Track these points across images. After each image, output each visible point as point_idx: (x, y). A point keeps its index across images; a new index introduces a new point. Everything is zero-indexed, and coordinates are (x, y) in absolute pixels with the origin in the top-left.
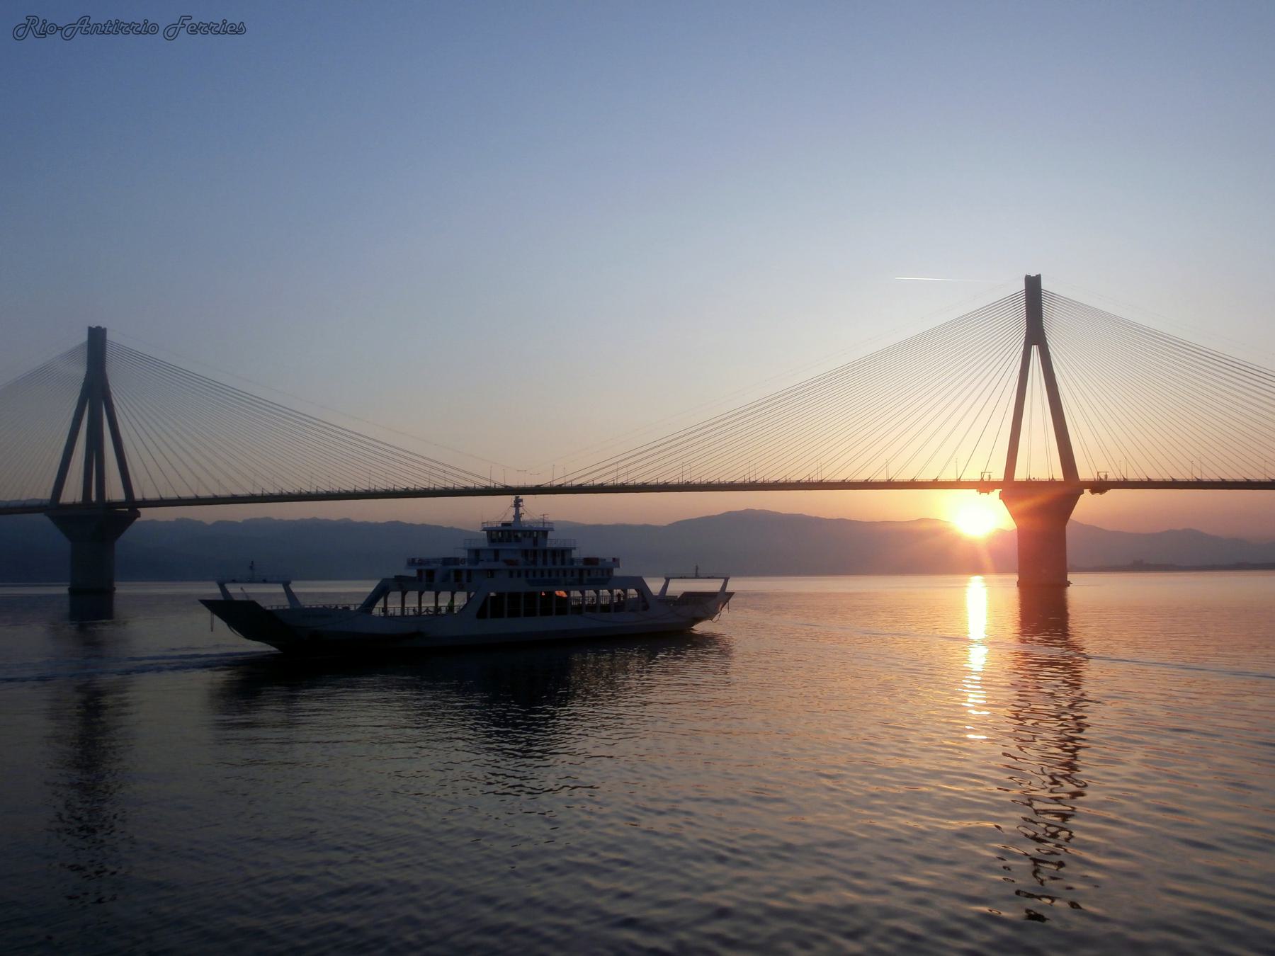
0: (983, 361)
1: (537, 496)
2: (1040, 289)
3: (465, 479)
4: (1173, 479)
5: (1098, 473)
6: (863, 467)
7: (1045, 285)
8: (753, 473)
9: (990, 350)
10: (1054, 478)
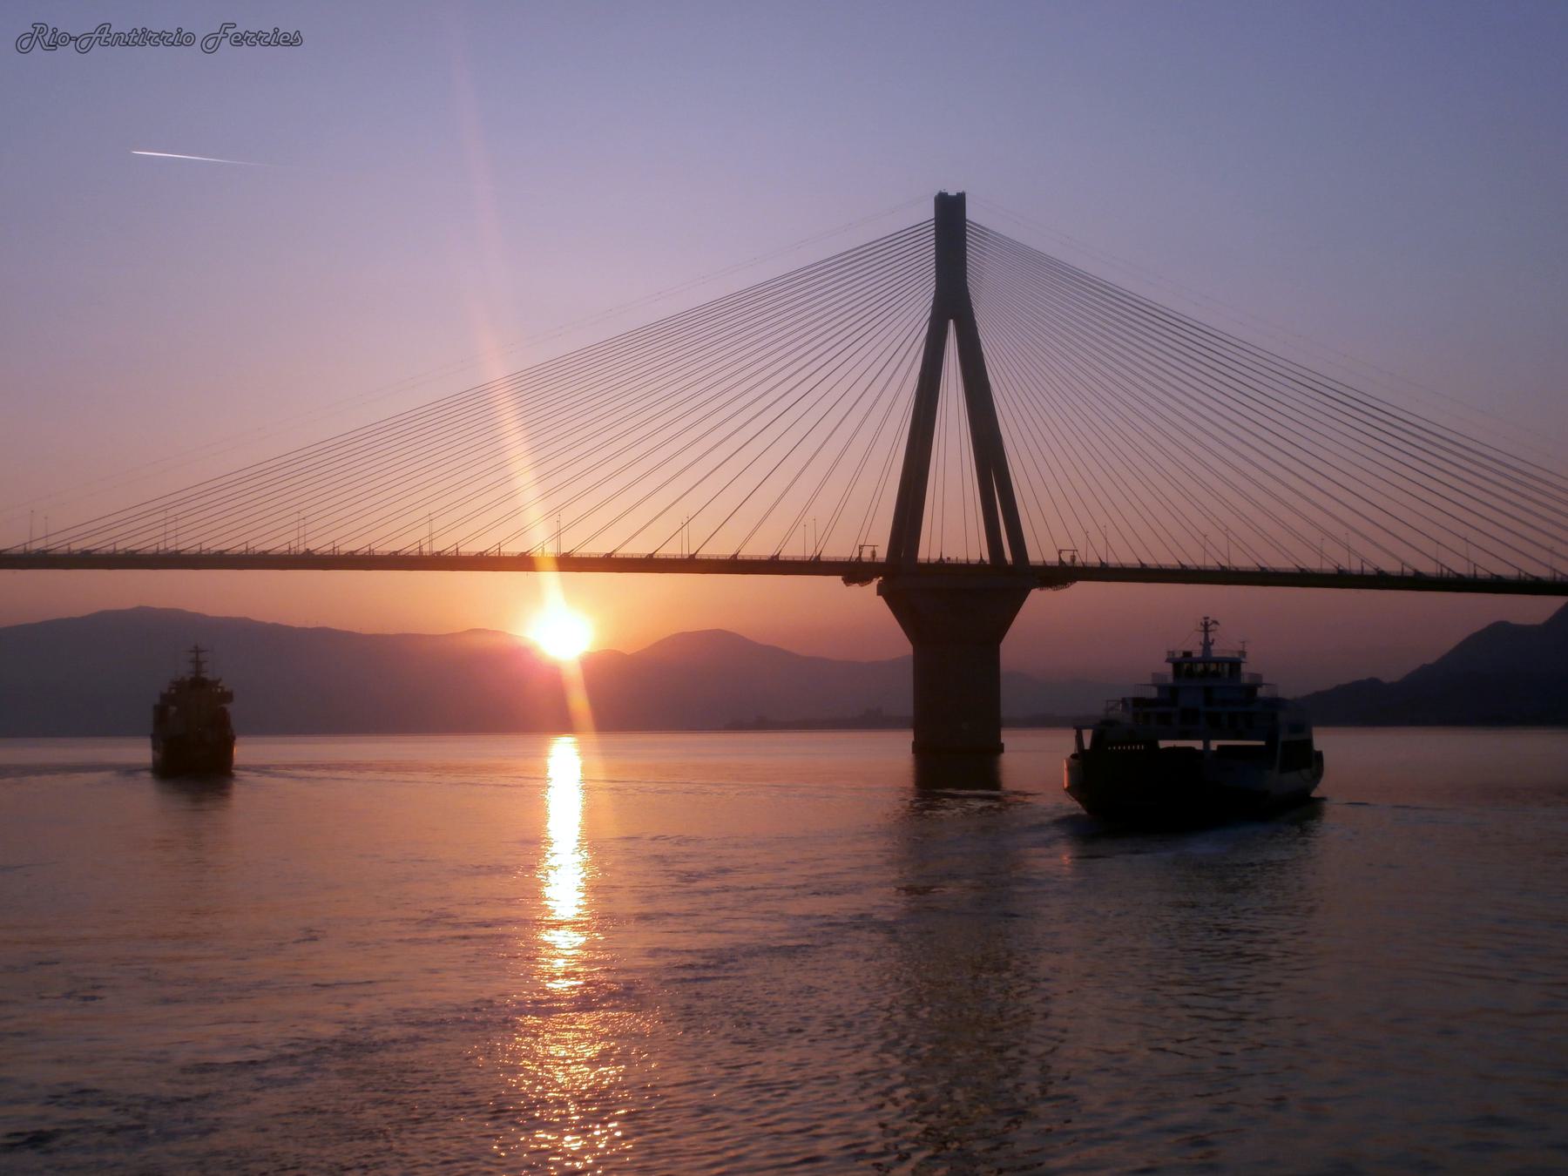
4: (1142, 564)
5: (1060, 552)
6: (113, 526)
7: (973, 213)
8: (302, 541)
9: (686, 342)
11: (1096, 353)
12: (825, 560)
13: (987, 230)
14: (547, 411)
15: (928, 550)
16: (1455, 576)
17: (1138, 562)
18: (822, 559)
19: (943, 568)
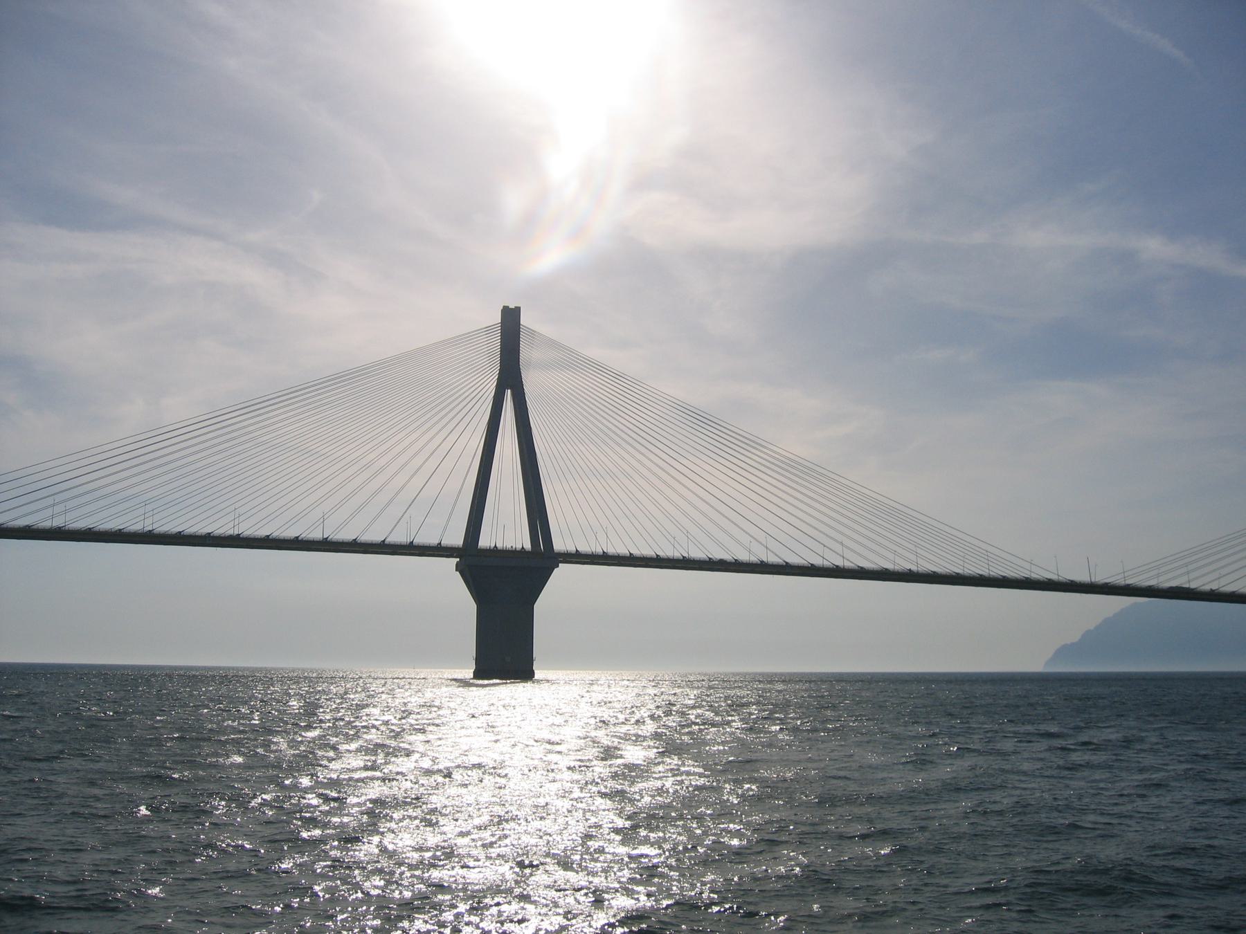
0: (423, 420)
1: (218, 548)
2: (520, 324)
3: (886, 559)
7: (524, 320)
9: (485, 375)
10: (524, 547)
11: (588, 403)
12: (445, 546)
13: (535, 332)
14: (886, 517)
15: (485, 541)
16: (832, 566)
17: (680, 555)
18: (442, 545)
19: (495, 553)
